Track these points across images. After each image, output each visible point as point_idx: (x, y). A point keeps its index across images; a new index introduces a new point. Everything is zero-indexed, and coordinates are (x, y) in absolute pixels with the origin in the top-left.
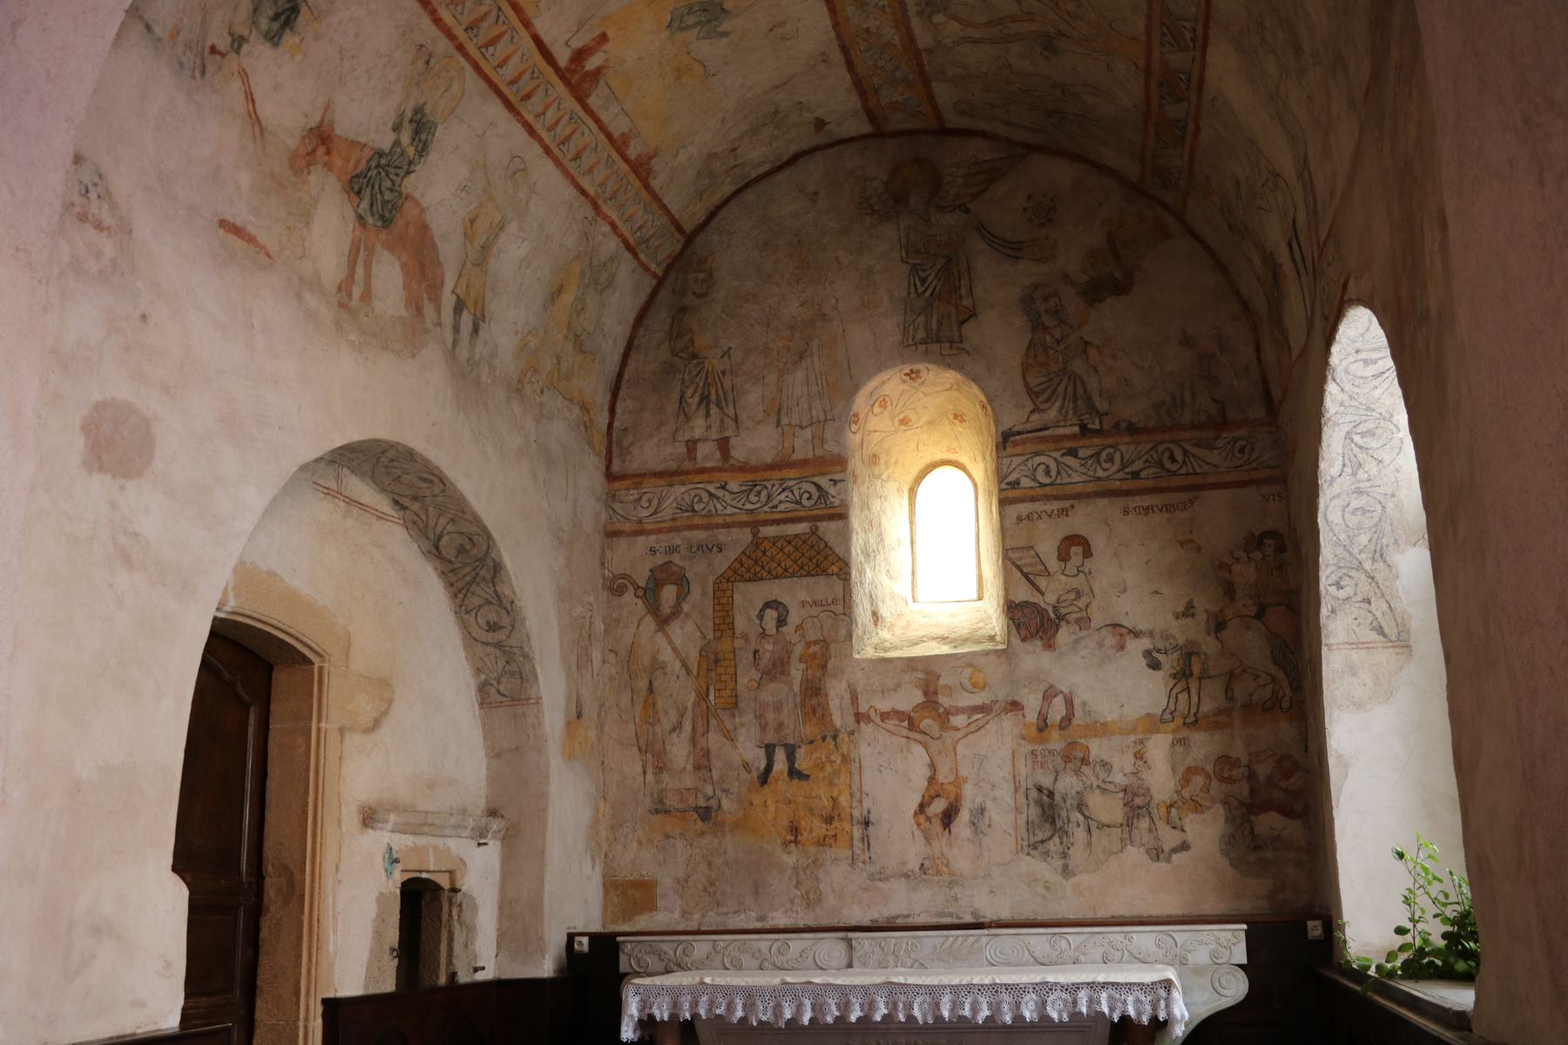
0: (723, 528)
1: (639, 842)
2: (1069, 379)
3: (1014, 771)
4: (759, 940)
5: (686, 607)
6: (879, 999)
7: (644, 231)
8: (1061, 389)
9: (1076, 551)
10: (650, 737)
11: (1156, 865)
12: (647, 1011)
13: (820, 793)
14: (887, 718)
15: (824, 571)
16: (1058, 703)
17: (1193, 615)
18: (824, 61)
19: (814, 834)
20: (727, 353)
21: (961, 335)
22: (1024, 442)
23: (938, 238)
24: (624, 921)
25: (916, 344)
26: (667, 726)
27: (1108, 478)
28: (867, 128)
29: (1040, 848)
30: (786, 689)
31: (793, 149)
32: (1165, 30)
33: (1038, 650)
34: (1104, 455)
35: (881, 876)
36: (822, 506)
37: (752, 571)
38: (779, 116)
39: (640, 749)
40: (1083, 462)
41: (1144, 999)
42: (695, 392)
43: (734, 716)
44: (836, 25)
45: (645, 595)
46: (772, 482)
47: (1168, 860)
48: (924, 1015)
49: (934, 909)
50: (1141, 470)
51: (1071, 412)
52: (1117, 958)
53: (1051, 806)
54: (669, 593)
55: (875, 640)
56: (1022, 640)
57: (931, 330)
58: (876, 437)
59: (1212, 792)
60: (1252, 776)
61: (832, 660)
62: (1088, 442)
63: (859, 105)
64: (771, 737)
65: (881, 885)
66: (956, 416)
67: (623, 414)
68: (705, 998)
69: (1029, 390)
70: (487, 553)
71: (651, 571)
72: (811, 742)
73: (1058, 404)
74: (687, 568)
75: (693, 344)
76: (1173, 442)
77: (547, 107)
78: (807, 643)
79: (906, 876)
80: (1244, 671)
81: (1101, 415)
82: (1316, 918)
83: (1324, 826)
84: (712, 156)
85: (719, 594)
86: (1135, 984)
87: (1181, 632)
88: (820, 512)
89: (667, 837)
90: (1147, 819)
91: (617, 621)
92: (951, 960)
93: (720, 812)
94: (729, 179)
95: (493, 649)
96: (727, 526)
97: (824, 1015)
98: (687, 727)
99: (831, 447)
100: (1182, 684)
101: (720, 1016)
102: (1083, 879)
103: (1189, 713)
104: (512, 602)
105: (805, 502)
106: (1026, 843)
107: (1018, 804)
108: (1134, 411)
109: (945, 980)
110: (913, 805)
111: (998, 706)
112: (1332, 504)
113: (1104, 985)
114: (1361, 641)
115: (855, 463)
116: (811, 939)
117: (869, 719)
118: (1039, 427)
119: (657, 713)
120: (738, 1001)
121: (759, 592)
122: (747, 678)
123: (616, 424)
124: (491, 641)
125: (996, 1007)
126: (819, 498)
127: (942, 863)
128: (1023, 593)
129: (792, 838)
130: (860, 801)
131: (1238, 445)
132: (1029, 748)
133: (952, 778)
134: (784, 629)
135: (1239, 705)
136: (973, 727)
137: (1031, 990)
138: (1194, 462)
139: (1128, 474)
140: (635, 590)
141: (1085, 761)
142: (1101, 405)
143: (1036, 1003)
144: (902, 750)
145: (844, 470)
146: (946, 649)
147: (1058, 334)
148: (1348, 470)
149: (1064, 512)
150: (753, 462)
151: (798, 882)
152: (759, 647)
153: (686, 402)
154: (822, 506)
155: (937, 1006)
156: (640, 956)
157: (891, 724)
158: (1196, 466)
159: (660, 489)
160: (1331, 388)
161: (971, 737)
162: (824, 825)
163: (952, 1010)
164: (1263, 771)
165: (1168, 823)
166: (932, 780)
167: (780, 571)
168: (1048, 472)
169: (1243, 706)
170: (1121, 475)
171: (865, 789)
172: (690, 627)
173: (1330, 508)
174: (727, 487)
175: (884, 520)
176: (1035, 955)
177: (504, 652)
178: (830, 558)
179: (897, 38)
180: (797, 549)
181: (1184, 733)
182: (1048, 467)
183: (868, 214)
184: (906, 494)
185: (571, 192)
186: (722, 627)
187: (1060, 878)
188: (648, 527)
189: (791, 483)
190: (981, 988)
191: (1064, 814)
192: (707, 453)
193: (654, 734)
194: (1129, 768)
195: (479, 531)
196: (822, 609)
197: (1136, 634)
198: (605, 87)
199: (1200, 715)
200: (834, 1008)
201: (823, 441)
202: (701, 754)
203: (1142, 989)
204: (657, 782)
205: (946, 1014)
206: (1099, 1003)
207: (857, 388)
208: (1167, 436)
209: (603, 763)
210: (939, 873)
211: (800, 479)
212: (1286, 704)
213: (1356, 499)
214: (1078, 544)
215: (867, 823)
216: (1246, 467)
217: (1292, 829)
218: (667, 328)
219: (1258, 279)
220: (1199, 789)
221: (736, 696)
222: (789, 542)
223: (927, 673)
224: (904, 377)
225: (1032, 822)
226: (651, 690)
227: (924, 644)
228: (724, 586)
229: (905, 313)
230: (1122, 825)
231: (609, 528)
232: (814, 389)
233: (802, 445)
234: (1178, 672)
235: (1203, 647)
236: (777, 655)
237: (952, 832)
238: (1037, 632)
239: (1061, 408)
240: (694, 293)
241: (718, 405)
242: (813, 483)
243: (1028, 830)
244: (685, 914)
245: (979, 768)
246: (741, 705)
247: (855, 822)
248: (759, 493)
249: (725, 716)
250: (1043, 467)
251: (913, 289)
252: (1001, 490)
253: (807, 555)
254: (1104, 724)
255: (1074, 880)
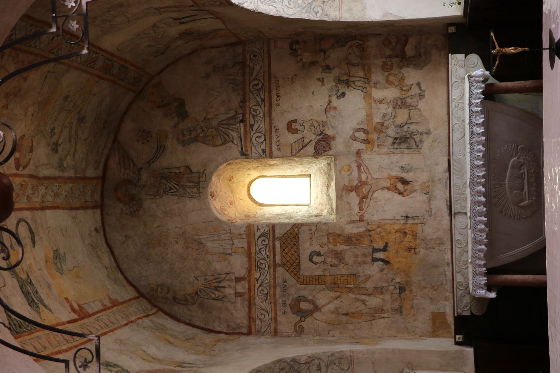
0: (276, 280)
1: (415, 320)
2: (220, 127)
3: (386, 154)
4: (455, 253)
5: (310, 297)
6: (476, 189)
7: (140, 310)
8: (224, 130)
9: (294, 126)
10: (367, 315)
11: (426, 96)
12: (483, 287)
13: (393, 238)
14: (362, 208)
15: (297, 235)
16: (358, 135)
17: (323, 78)
18: (75, 218)
19: (411, 240)
20: (196, 278)
21: (197, 173)
22: (246, 147)
23: (152, 182)
24: (450, 328)
25: (199, 193)
26: (363, 307)
27: (264, 112)
28: (98, 211)
29: (418, 144)
30: (348, 252)
31: (105, 245)
32: (89, 66)
33: (335, 143)
34: (254, 113)
35: (430, 212)
36: (268, 235)
37: (295, 267)
38: (93, 244)
39: (373, 320)
40: (256, 122)
41: (475, 86)
42: (213, 293)
43: (359, 276)
44: (63, 208)
45: (304, 317)
46: (256, 258)
47: (424, 91)
48: (482, 171)
49: (444, 189)
50: (261, 98)
51: (234, 126)
52: (462, 105)
53: (401, 139)
54: (304, 306)
55: (328, 215)
56: (331, 149)
57: (193, 186)
58: (237, 215)
59: (396, 73)
60: (390, 57)
61: (336, 231)
62: (248, 120)
63: (91, 210)
64: (369, 259)
65: (433, 212)
66: (230, 180)
67: (221, 327)
68: (477, 262)
69: (223, 144)
70: (288, 363)
71: (293, 314)
72: (372, 241)
73: (230, 132)
74: (293, 297)
75: (191, 294)
76: (250, 84)
77: (94, 327)
78: (328, 243)
79: (430, 200)
80: (347, 58)
81: (236, 113)
82: (447, 30)
83: (411, 26)
84: (108, 276)
85: (305, 282)
86: (469, 89)
87: (330, 83)
88: (271, 236)
89: (412, 307)
90: (407, 99)
91: (315, 330)
92: (463, 171)
93: (401, 283)
94: (116, 274)
95: (329, 370)
96: (275, 278)
97: (483, 212)
98: (363, 297)
99: (243, 231)
100: (352, 84)
101: (484, 255)
102: (431, 126)
103: (363, 81)
104: (309, 357)
105: (266, 243)
106: (416, 150)
107: (400, 152)
108: (235, 100)
109: (468, 163)
110: (399, 197)
111: (358, 160)
112: (286, 12)
113: (470, 101)
114: (339, 6)
115: (250, 221)
116: (455, 230)
117: (362, 216)
118: (240, 140)
119: (357, 312)
120: (478, 247)
121: (305, 264)
122: (343, 270)
123: (225, 330)
124: (325, 370)
125: (479, 143)
126: (265, 236)
127: (424, 185)
128: (310, 149)
129: (413, 250)
130: (397, 220)
131: (253, 58)
132: (376, 147)
133: (388, 180)
134: (322, 253)
135: (361, 61)
136: (367, 171)
137: (472, 129)
138: (259, 76)
139: (262, 104)
140: (302, 321)
141: (382, 124)
142: (232, 113)
143: (477, 127)
144: (376, 202)
145: (253, 225)
146: (333, 184)
147: (200, 131)
148: (274, 4)
149: (277, 131)
150: (247, 266)
151: (432, 248)
152: (329, 265)
153: (218, 297)
154: (268, 235)
155: (479, 166)
156: (463, 306)
157: (364, 206)
158: (260, 75)
159: (256, 309)
160: (245, 6)
161: (371, 172)
162: (407, 236)
163: (480, 160)
164: (388, 52)
165: (409, 91)
166: (389, 189)
167: (296, 254)
168: (260, 137)
169: (361, 60)
170: (262, 106)
171: (392, 218)
172: (319, 296)
173: (287, 13)
174: (257, 278)
175: (275, 213)
176: (461, 137)
177: (330, 364)
178: (292, 232)
179: (70, 185)
180: (287, 247)
181: (372, 84)
182: (257, 137)
183: (138, 212)
184: (261, 207)
185: (127, 327)
186: (320, 281)
187: (431, 136)
188: (273, 315)
189: (257, 249)
190: (471, 149)
191: (404, 134)
192: (241, 288)
193: (366, 313)
194: (386, 106)
195: (278, 364)
196: (314, 236)
197: (330, 102)
198: (84, 305)
199: (365, 77)
200: (480, 208)
201: (240, 234)
202: (376, 291)
203: (472, 87)
204: (388, 312)
205: (482, 162)
206: (477, 103)
207: (217, 219)
208: (247, 87)
209: (379, 337)
210: (428, 187)
211: (256, 245)
212: (361, 42)
213: (285, 3)
214: (291, 125)
215: (407, 217)
216: (262, 55)
217: (412, 42)
218: (182, 306)
219: (186, 43)
220: (395, 78)
221: (351, 275)
222: (284, 250)
223: (343, 190)
224: (213, 199)
225: (407, 147)
226: (347, 314)
227: (330, 194)
228: (302, 280)
229: (185, 197)
230: (409, 110)
231: (273, 334)
232: (216, 238)
233: (241, 244)
234: (347, 85)
235: (336, 75)
236: (333, 256)
237: (411, 180)
238: (328, 143)
239: (232, 130)
240: (167, 293)
241: (220, 282)
242: (258, 239)
243: (411, 149)
244: (446, 299)
245: (384, 169)
246: (354, 273)
247: (406, 223)
248: (261, 263)
249: (359, 280)
250: (257, 139)
251: (174, 194)
252: (266, 157)
253: (290, 242)
254: (367, 116)
255: (432, 130)
